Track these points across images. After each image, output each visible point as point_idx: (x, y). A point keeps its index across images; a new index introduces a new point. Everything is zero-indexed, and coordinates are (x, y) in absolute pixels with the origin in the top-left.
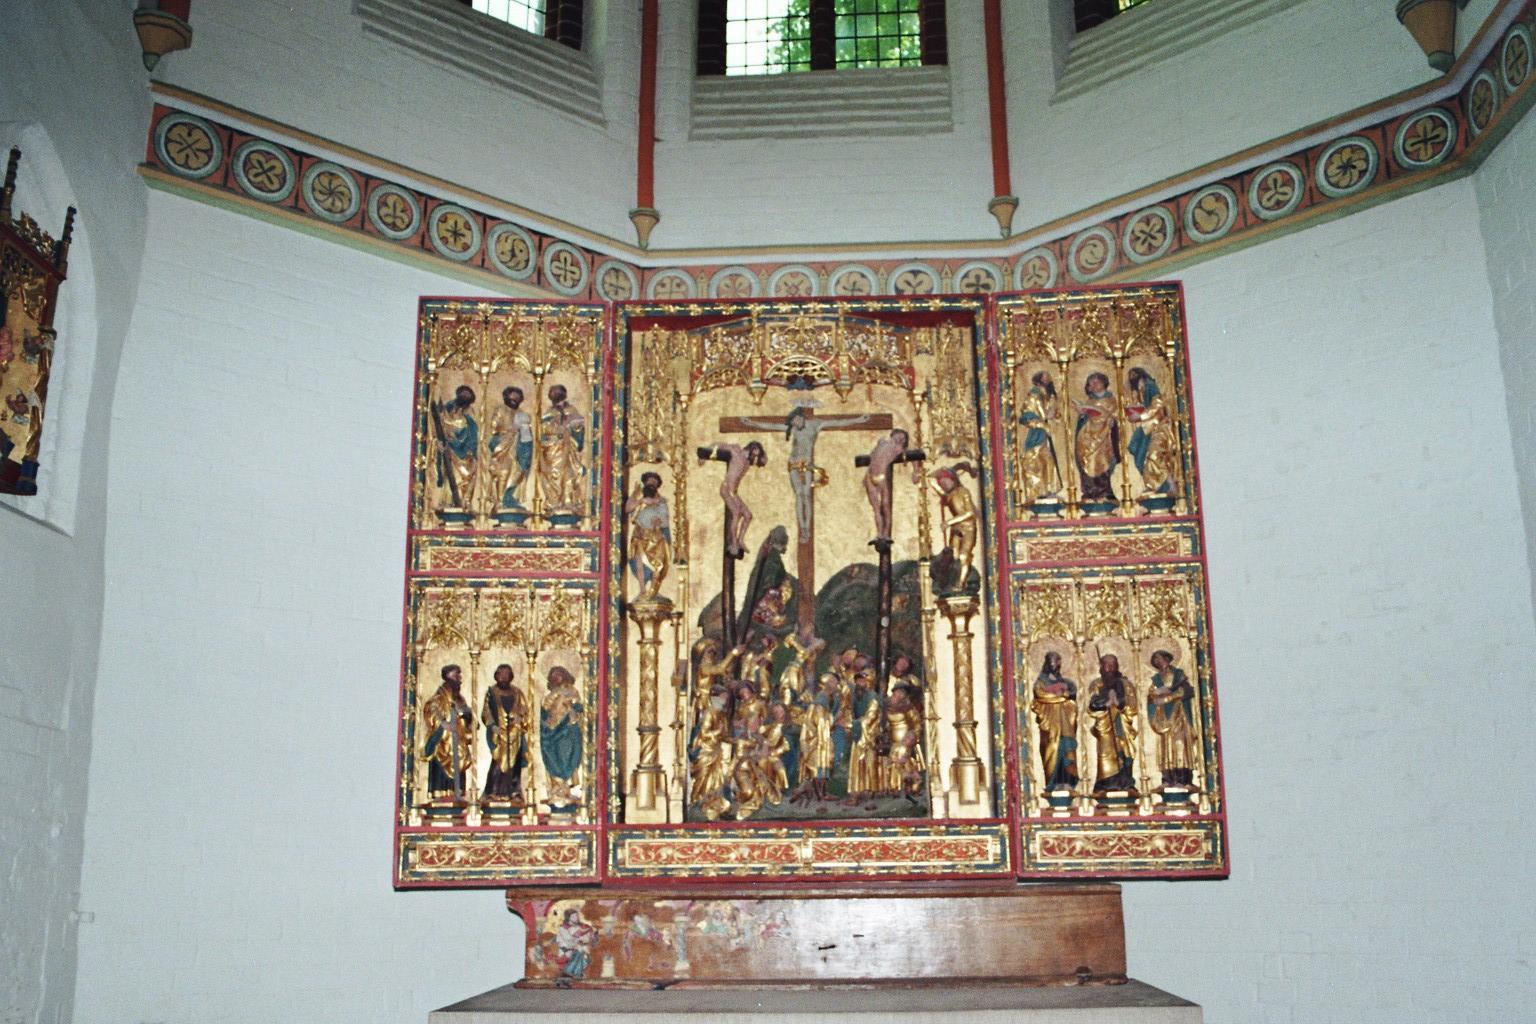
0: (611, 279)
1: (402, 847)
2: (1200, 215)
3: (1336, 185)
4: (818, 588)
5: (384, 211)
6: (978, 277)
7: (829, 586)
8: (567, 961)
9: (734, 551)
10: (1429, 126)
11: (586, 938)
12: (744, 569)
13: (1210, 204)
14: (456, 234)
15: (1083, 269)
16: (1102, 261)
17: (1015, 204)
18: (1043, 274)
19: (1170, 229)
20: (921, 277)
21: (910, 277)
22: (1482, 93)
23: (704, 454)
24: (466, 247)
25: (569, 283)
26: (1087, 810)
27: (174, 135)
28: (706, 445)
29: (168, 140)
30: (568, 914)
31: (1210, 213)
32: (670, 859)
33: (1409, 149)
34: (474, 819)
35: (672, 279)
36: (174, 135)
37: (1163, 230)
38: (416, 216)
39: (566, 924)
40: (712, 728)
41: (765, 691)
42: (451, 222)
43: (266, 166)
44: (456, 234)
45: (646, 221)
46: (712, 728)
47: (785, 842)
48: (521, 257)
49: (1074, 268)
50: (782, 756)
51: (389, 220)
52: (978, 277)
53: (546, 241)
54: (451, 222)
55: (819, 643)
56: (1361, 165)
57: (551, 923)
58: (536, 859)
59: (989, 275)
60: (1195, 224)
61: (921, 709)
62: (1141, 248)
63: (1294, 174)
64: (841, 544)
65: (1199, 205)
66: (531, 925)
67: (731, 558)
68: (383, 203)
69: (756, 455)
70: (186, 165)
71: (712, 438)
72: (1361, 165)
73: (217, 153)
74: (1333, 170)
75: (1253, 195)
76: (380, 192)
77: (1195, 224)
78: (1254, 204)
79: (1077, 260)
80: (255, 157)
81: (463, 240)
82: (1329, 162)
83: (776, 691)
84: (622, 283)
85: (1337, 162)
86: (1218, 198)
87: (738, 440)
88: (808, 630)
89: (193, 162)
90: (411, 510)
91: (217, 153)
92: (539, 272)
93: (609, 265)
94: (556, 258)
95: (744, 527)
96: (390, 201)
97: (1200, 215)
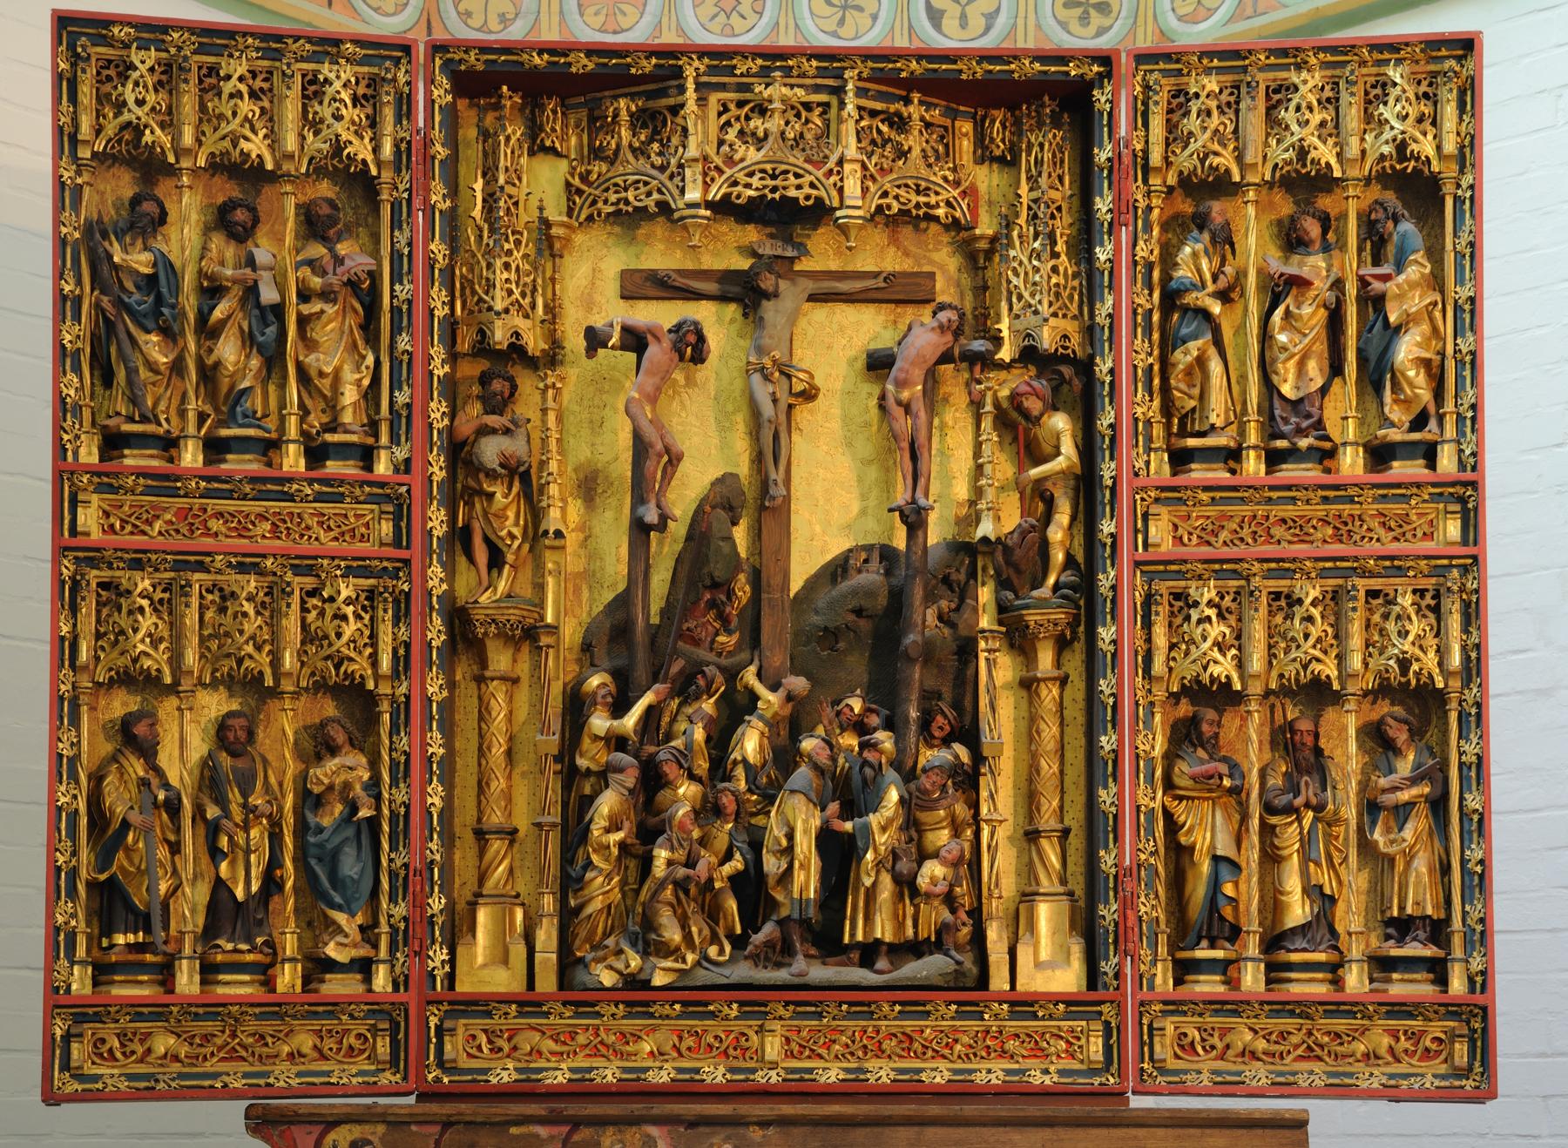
9: (651, 516)
12: (665, 552)
26: (1252, 978)
34: (187, 980)
41: (702, 765)
55: (799, 684)
69: (691, 346)
87: (661, 315)
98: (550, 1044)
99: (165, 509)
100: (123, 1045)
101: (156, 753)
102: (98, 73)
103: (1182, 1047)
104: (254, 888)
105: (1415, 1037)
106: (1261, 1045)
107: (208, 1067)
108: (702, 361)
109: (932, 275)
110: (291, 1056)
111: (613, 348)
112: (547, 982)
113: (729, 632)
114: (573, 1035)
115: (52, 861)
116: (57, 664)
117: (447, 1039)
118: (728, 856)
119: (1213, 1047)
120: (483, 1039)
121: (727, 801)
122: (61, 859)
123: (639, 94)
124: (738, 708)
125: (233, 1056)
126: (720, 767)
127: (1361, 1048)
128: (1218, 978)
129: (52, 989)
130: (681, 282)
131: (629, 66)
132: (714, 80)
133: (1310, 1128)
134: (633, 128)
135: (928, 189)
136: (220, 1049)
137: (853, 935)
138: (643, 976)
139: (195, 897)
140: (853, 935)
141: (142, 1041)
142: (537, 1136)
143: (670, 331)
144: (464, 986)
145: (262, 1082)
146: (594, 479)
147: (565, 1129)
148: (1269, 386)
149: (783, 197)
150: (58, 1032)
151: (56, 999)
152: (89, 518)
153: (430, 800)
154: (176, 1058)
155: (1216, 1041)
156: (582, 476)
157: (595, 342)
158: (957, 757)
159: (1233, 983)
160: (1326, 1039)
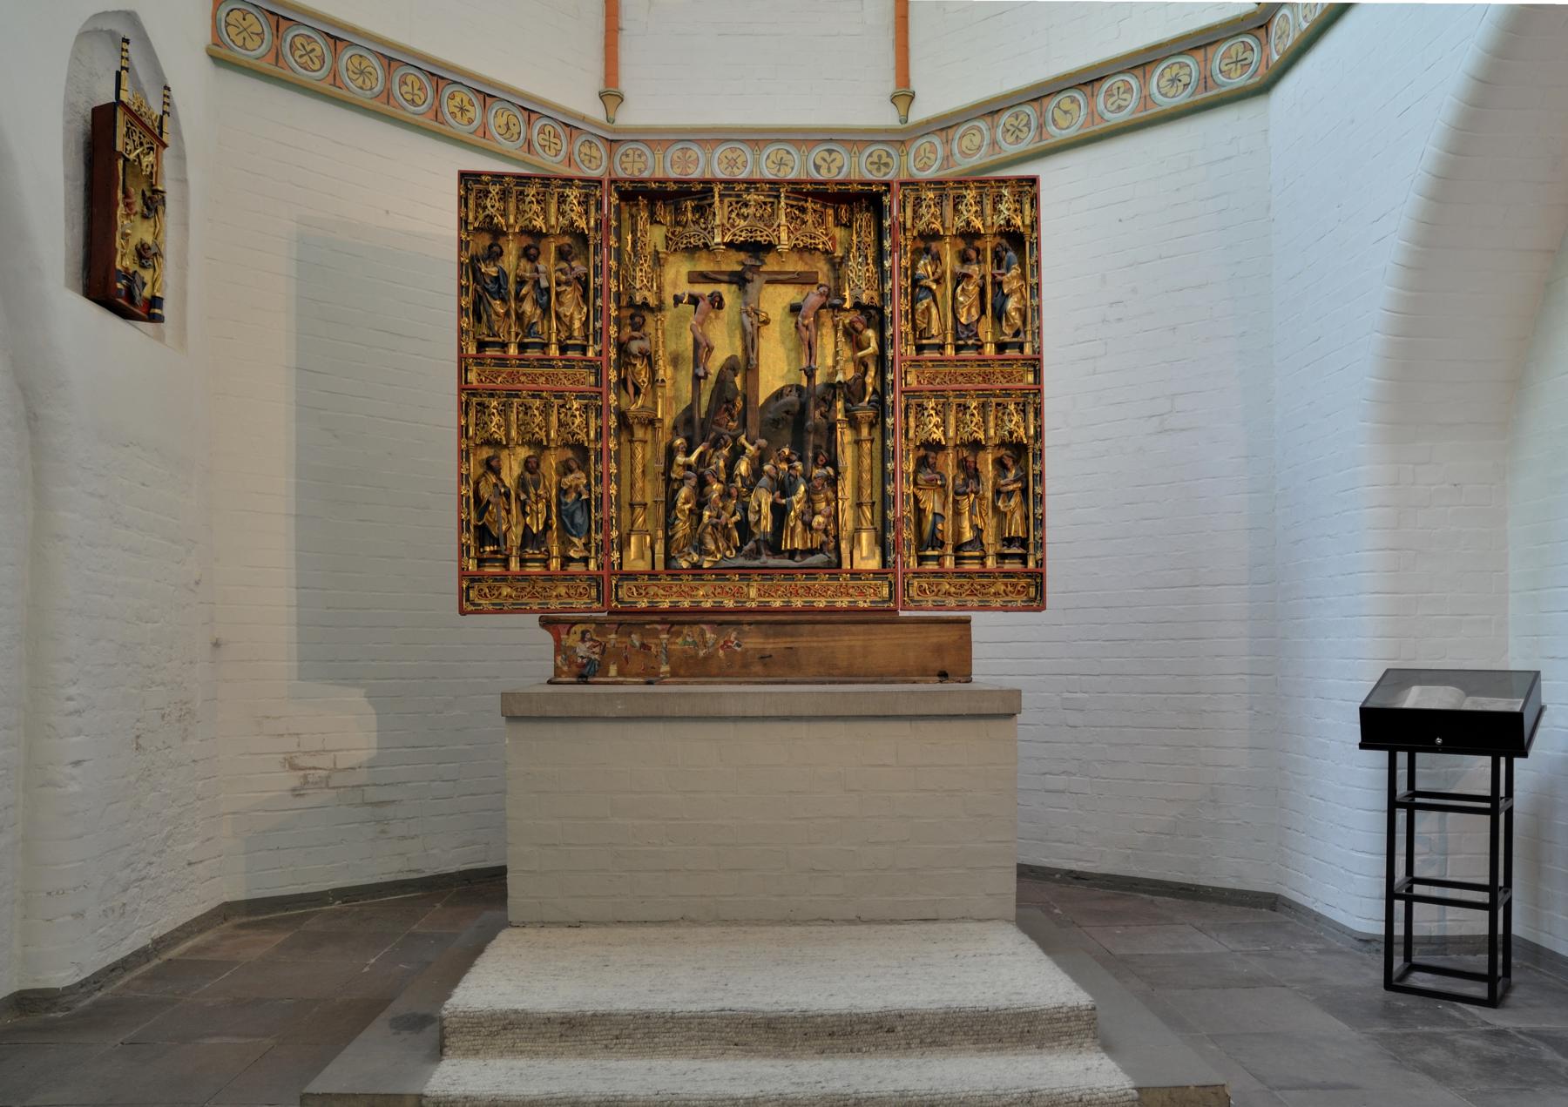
0: (585, 150)
1: (772, 562)
2: (1058, 113)
3: (1165, 95)
4: (761, 401)
5: (405, 89)
6: (880, 157)
7: (768, 401)
8: (584, 666)
9: (701, 373)
10: (1241, 50)
11: (597, 650)
12: (707, 388)
13: (1066, 105)
14: (462, 109)
15: (963, 153)
16: (979, 148)
17: (912, 97)
18: (932, 156)
19: (1034, 124)
20: (834, 155)
21: (826, 155)
22: (1283, 24)
23: (677, 300)
24: (471, 121)
25: (553, 152)
26: (949, 563)
27: (231, 19)
28: (679, 293)
29: (227, 24)
30: (584, 633)
31: (1066, 112)
32: (656, 595)
33: (1224, 68)
34: (514, 565)
35: (634, 150)
36: (231, 19)
37: (1028, 125)
38: (430, 93)
39: (583, 640)
40: (687, 502)
41: (723, 476)
42: (458, 99)
43: (309, 48)
44: (462, 109)
45: (611, 101)
46: (687, 502)
47: (738, 584)
48: (514, 130)
49: (956, 150)
50: (737, 524)
51: (409, 97)
52: (880, 157)
53: (533, 116)
54: (458, 99)
55: (763, 442)
56: (1185, 79)
57: (572, 640)
58: (558, 599)
59: (889, 155)
60: (1054, 120)
61: (836, 493)
62: (1011, 139)
63: (1134, 83)
64: (775, 371)
65: (1058, 105)
66: (558, 641)
67: (697, 379)
68: (403, 83)
69: (717, 302)
70: (244, 47)
71: (685, 289)
72: (1185, 79)
73: (267, 36)
74: (1163, 83)
75: (1101, 99)
76: (559, 158)
77: (1054, 120)
78: (1101, 106)
79: (960, 145)
80: (298, 41)
81: (468, 115)
82: (1162, 75)
83: (730, 477)
84: (594, 153)
85: (1168, 75)
86: (1073, 100)
87: (705, 290)
88: (754, 432)
89: (249, 44)
90: (460, 340)
91: (267, 36)
92: (529, 143)
93: (583, 138)
94: (542, 131)
95: (708, 356)
96: (409, 79)
97: (1058, 113)
112: (660, 566)
121: (733, 491)
152: (472, 377)
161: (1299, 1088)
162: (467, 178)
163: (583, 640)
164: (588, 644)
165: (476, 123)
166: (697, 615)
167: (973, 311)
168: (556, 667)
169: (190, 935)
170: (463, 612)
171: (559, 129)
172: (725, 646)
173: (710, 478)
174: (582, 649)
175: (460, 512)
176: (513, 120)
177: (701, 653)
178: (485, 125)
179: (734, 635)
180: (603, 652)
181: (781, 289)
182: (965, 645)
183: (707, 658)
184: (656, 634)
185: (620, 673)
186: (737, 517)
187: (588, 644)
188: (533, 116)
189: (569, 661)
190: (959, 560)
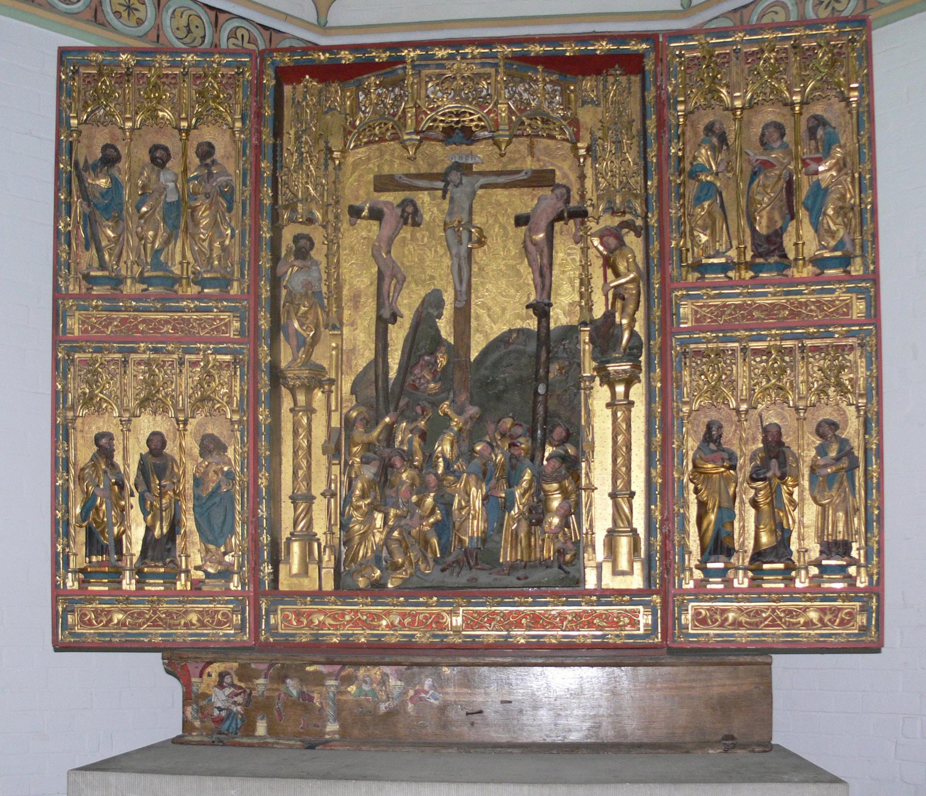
4: (474, 355)
8: (220, 720)
9: (386, 314)
11: (239, 699)
12: (398, 335)
14: (129, 8)
24: (140, 22)
26: (741, 581)
30: (222, 675)
32: (322, 625)
34: (128, 584)
39: (221, 685)
41: (418, 459)
46: (363, 497)
47: (436, 610)
53: (222, 17)
55: (473, 410)
57: (205, 684)
69: (410, 215)
87: (391, 198)
98: (329, 621)
99: (114, 319)
100: (96, 618)
101: (112, 457)
102: (84, 80)
103: (698, 621)
104: (165, 531)
105: (836, 611)
106: (743, 619)
107: (142, 630)
108: (419, 225)
109: (553, 171)
110: (186, 625)
111: (364, 218)
112: (329, 585)
113: (435, 382)
114: (343, 616)
115: (54, 516)
116: (55, 408)
117: (272, 616)
118: (432, 512)
119: (717, 620)
120: (292, 617)
121: (432, 479)
122: (59, 515)
123: (381, 75)
124: (438, 427)
125: (155, 624)
126: (430, 459)
127: (802, 620)
128: (720, 580)
129: (55, 586)
130: (406, 181)
131: (374, 57)
132: (423, 63)
133: (773, 666)
134: (446, 414)
135: (548, 120)
136: (148, 620)
137: (505, 558)
138: (382, 582)
139: (137, 533)
140: (505, 558)
141: (106, 615)
142: (321, 673)
143: (398, 206)
144: (283, 586)
145: (171, 639)
146: (359, 296)
147: (338, 667)
148: (753, 230)
149: (463, 126)
150: (60, 609)
151: (57, 592)
152: (74, 325)
153: (260, 481)
154: (124, 625)
155: (718, 617)
156: (352, 294)
157: (355, 212)
158: (567, 451)
159: (728, 582)
160: (782, 615)
161: (645, 152)
162: (63, 52)
163: (221, 685)
164: (228, 691)
165: (147, 25)
166: (379, 652)
167: (777, 216)
168: (186, 724)
169: (877, 620)
170: (60, 647)
171: (255, 32)
172: (417, 698)
173: (397, 462)
174: (220, 698)
175: (54, 508)
176: (196, 22)
177: (383, 707)
178: (158, 27)
179: (428, 682)
180: (246, 704)
181: (501, 195)
182: (762, 697)
183: (390, 713)
184: (319, 679)
185: (271, 730)
186: (438, 515)
187: (228, 691)
188: (222, 17)
189: (202, 712)
190: (758, 575)
